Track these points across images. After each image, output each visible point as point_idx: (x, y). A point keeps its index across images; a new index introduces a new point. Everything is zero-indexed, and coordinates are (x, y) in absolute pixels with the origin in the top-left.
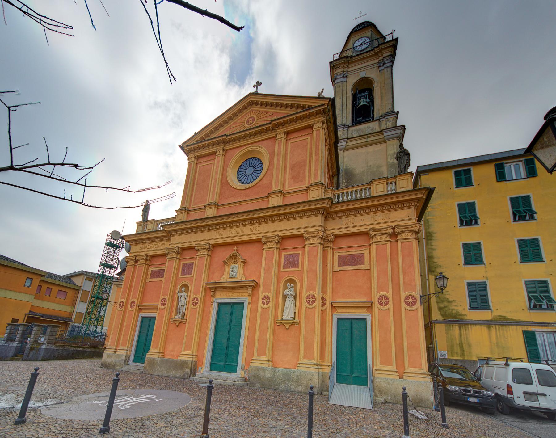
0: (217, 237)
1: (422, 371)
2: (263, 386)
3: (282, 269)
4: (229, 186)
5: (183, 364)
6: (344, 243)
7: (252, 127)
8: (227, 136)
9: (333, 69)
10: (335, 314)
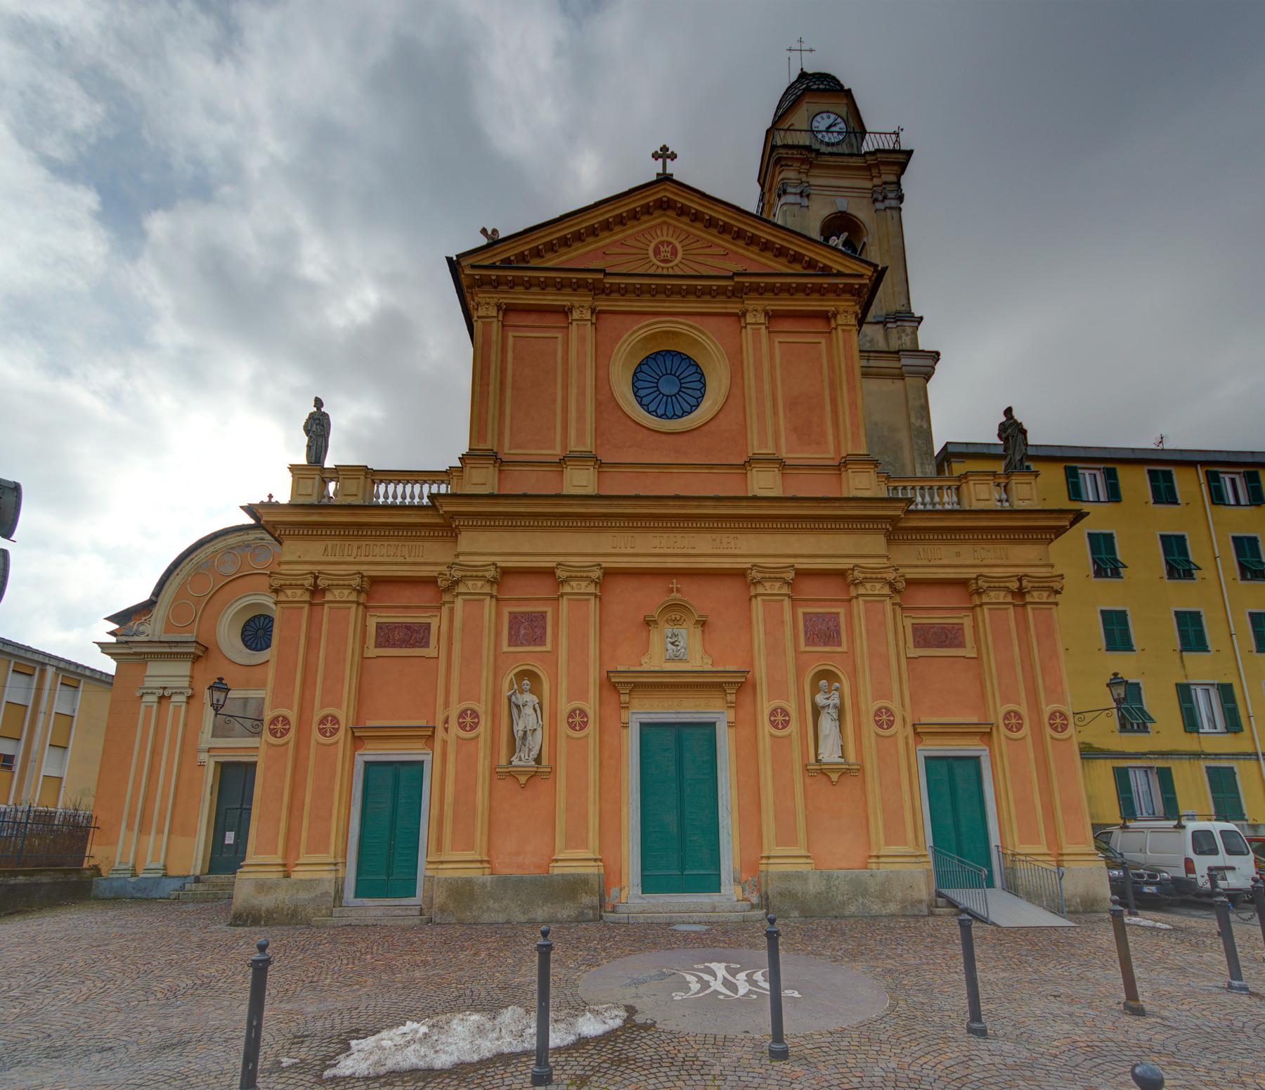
0: (616, 551)
2: (807, 913)
3: (803, 647)
5: (574, 886)
6: (924, 598)
8: (606, 274)
9: (776, 164)
10: (921, 748)
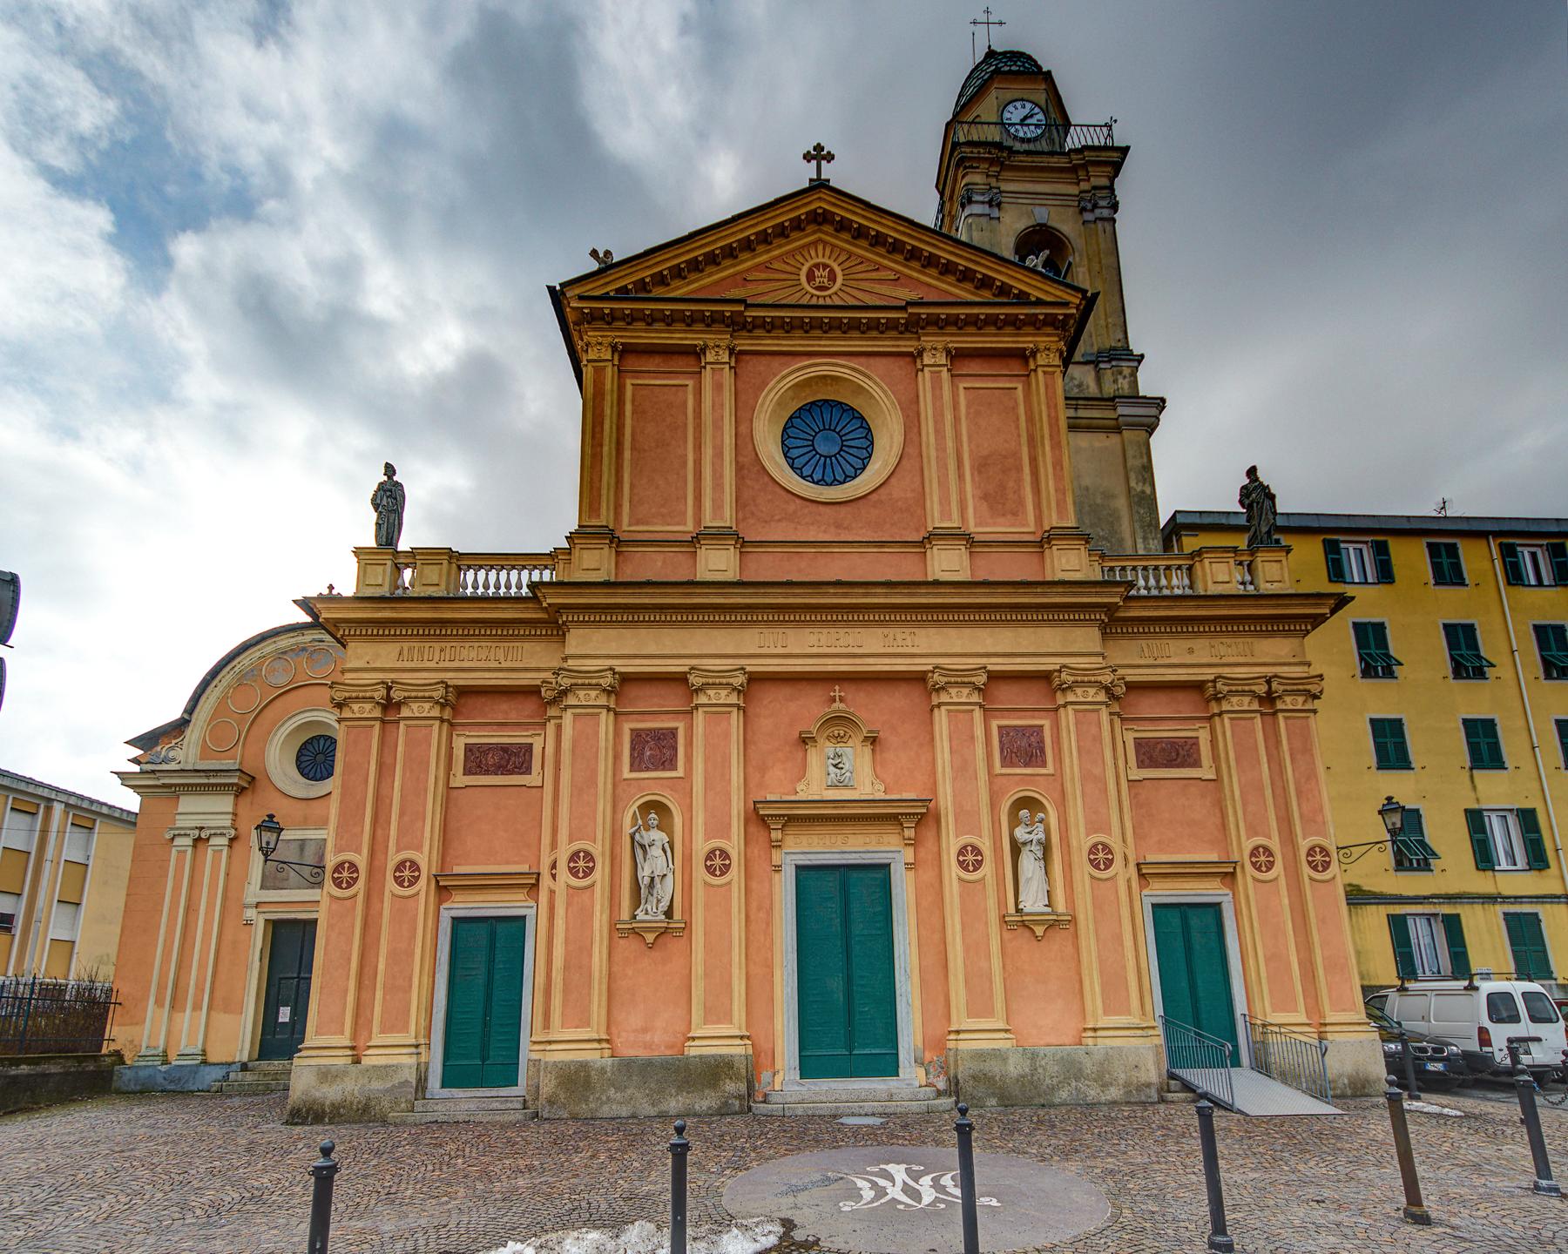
1: (1358, 1017)
2: (1007, 1101)
4: (766, 479)
6: (1149, 706)
7: (821, 302)
